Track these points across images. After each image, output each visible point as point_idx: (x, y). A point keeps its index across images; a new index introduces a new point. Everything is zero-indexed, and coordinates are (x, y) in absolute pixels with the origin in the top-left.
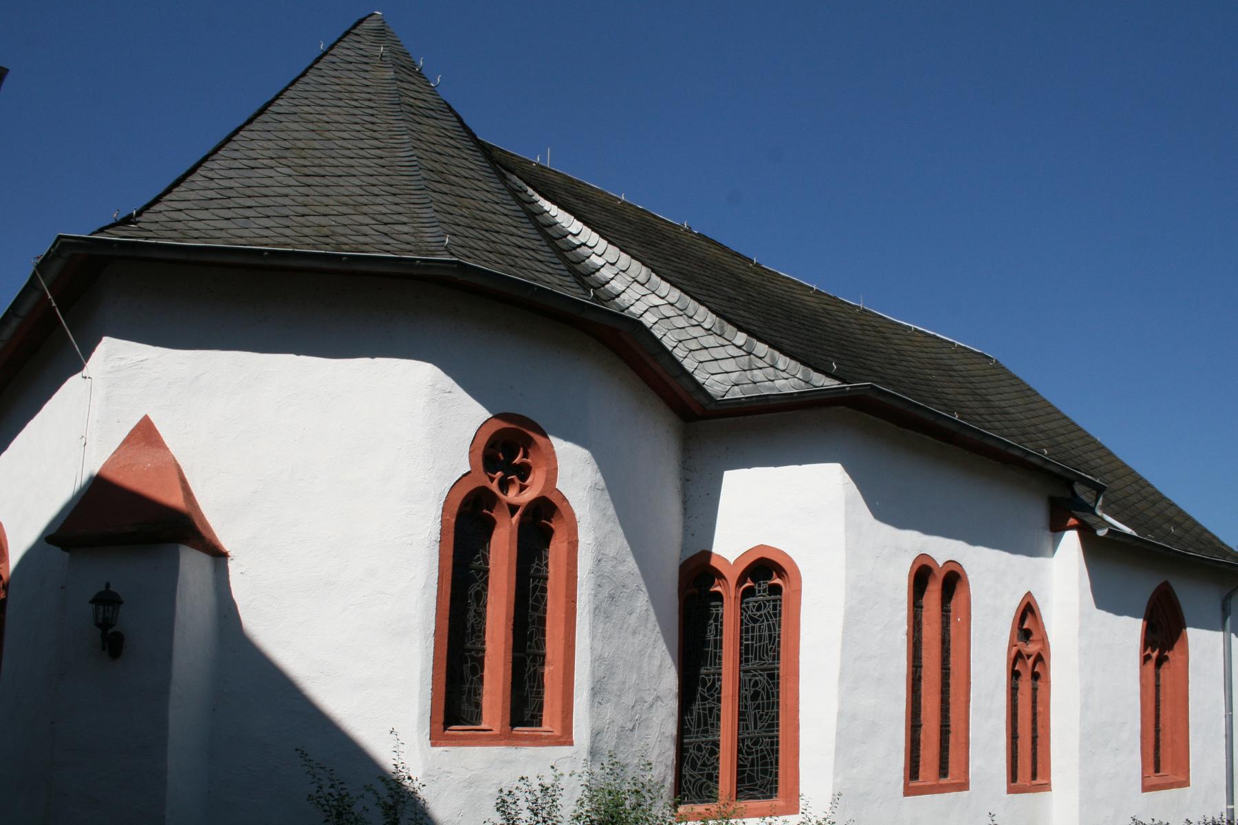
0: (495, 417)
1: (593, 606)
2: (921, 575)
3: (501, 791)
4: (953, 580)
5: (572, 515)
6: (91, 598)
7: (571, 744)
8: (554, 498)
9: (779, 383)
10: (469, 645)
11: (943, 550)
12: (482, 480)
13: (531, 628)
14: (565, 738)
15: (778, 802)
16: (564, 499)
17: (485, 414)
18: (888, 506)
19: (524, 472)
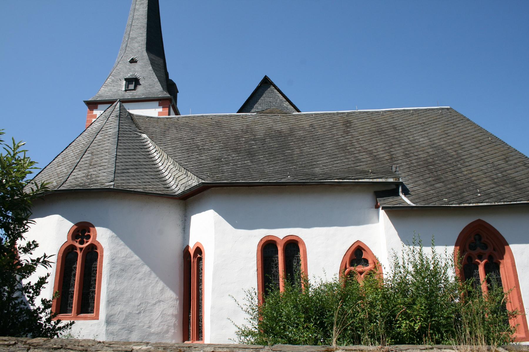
0: (76, 225)
1: (109, 275)
2: (268, 248)
3: (70, 328)
4: (293, 247)
5: (102, 247)
6: (127, 77)
7: (98, 319)
8: (95, 243)
9: (190, 183)
10: (70, 290)
11: (281, 234)
12: (71, 242)
13: (92, 283)
14: (97, 318)
15: (93, 315)
16: (99, 243)
17: (72, 224)
18: (238, 223)
19: (89, 237)
